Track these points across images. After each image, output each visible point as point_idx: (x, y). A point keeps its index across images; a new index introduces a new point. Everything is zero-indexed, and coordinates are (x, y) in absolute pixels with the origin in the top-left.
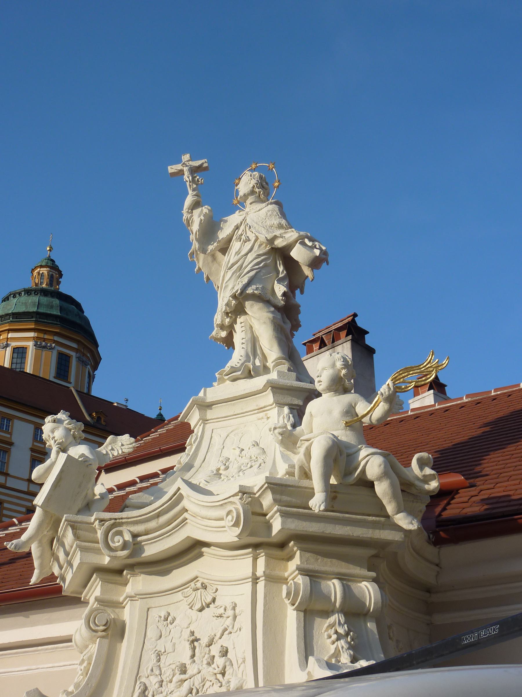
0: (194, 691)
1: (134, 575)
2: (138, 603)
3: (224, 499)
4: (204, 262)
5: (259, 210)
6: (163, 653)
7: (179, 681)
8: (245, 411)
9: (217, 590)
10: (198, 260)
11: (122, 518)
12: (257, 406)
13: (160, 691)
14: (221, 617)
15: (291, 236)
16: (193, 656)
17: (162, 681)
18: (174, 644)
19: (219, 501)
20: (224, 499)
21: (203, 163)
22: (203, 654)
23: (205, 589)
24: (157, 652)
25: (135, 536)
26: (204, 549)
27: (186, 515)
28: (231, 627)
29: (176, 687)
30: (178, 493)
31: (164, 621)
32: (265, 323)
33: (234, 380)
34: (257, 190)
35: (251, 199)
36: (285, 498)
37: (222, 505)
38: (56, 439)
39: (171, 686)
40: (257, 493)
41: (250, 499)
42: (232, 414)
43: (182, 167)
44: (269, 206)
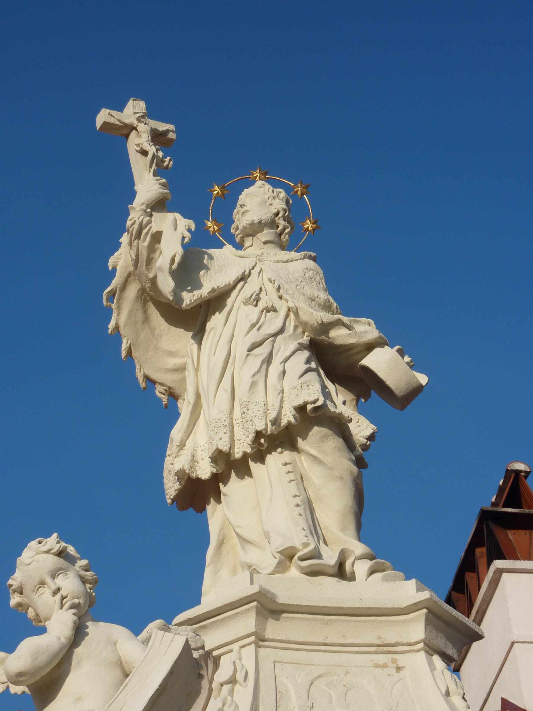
4: (129, 317)
5: (287, 261)
8: (349, 641)
10: (119, 308)
15: (366, 332)
21: (168, 131)
32: (341, 478)
33: (313, 573)
34: (282, 223)
35: (267, 234)
38: (63, 592)
40: (249, 644)
42: (321, 640)
43: (136, 122)
44: (307, 260)
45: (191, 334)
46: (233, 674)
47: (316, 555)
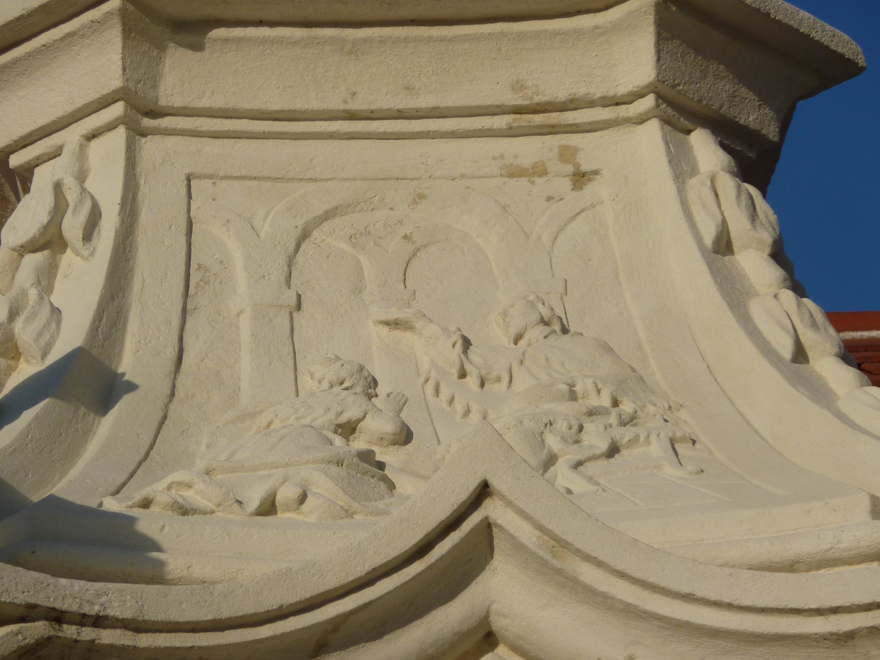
8: (424, 102)
11: (99, 621)
12: (518, 86)
19: (835, 610)
30: (475, 519)
42: (335, 103)
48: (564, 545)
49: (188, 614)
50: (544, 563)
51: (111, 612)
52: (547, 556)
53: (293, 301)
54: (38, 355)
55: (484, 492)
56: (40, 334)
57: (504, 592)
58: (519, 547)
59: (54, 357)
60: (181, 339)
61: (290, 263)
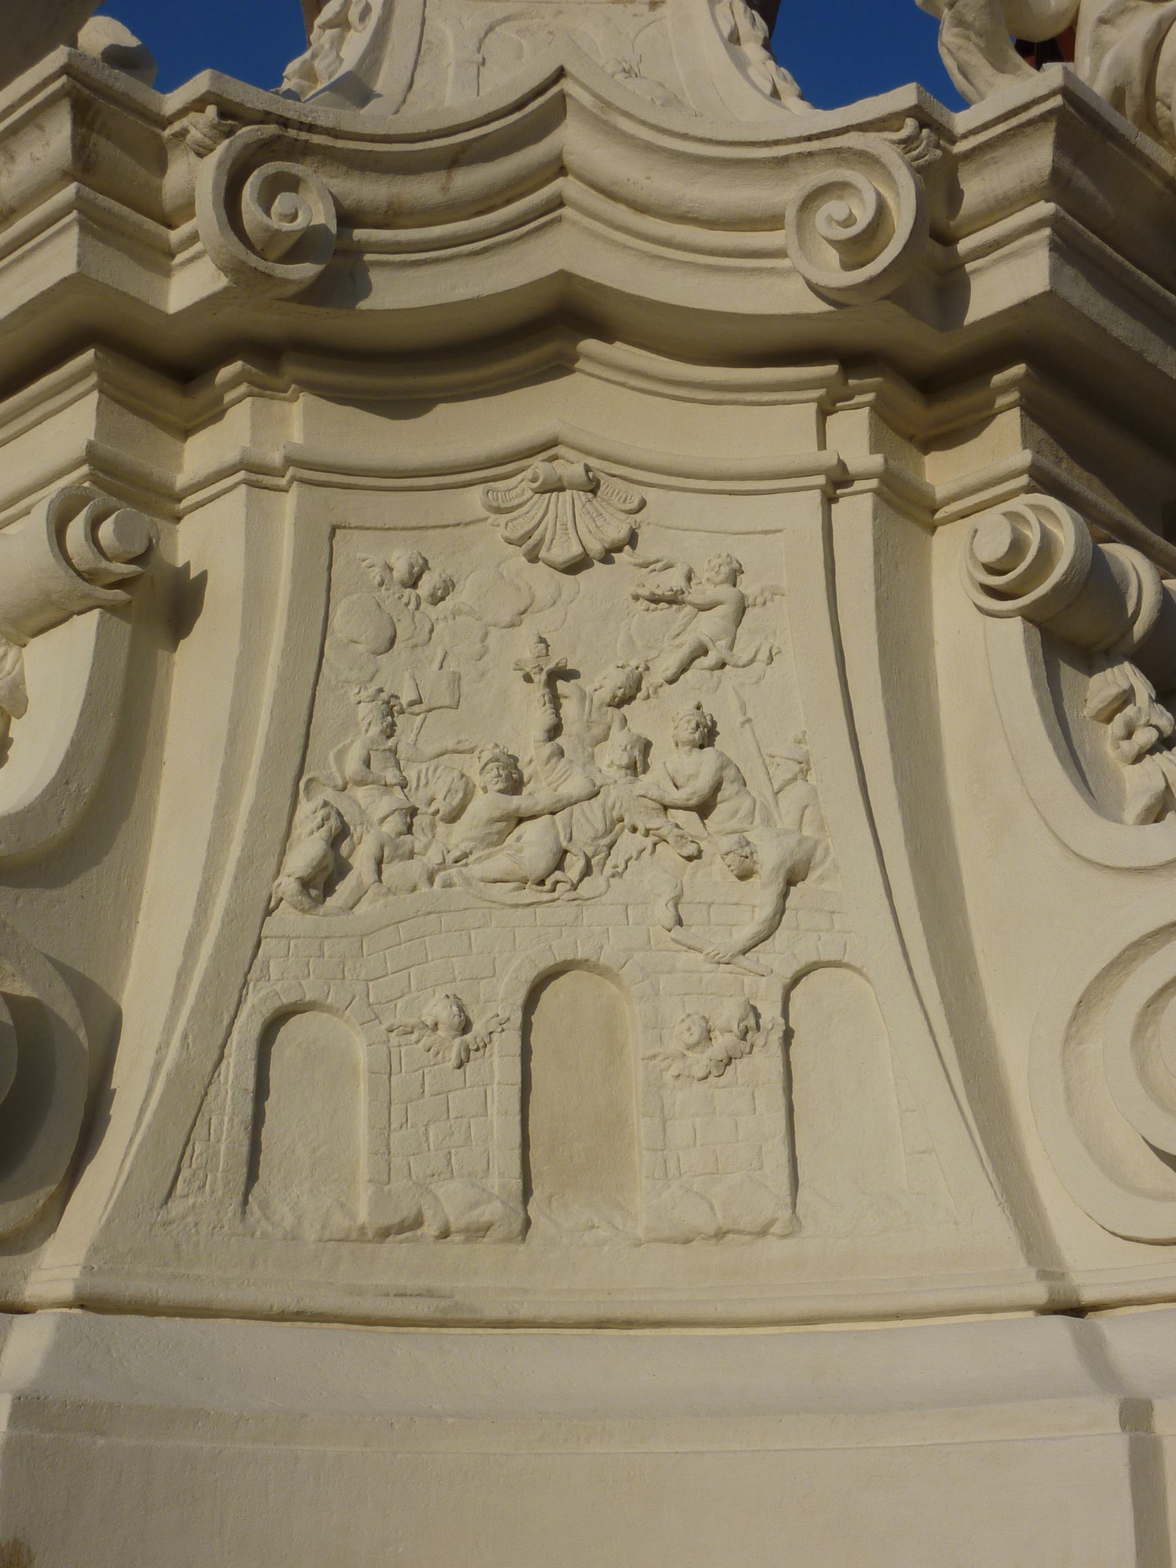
0: (574, 866)
1: (262, 389)
2: (289, 504)
3: (809, 138)
6: (412, 704)
7: (499, 820)
9: (643, 504)
13: (406, 848)
14: (671, 602)
16: (555, 731)
17: (413, 812)
18: (456, 679)
19: (777, 143)
20: (809, 138)
22: (597, 731)
23: (594, 491)
24: (384, 696)
25: (348, 218)
26: (590, 345)
27: (566, 186)
28: (723, 643)
29: (483, 839)
31: (405, 585)
36: (1083, 181)
37: (784, 161)
39: (460, 835)
40: (965, 136)
41: (938, 153)
45: (92, 438)
46: (341, 11)
47: (768, 821)
48: (608, 105)
49: (369, 130)
50: (596, 117)
51: (319, 123)
52: (599, 113)
53: (481, 60)
54: (326, 76)
55: (561, 74)
56: (329, 65)
57: (571, 138)
58: (582, 108)
59: (333, 79)
60: (413, 76)
61: (481, 42)
